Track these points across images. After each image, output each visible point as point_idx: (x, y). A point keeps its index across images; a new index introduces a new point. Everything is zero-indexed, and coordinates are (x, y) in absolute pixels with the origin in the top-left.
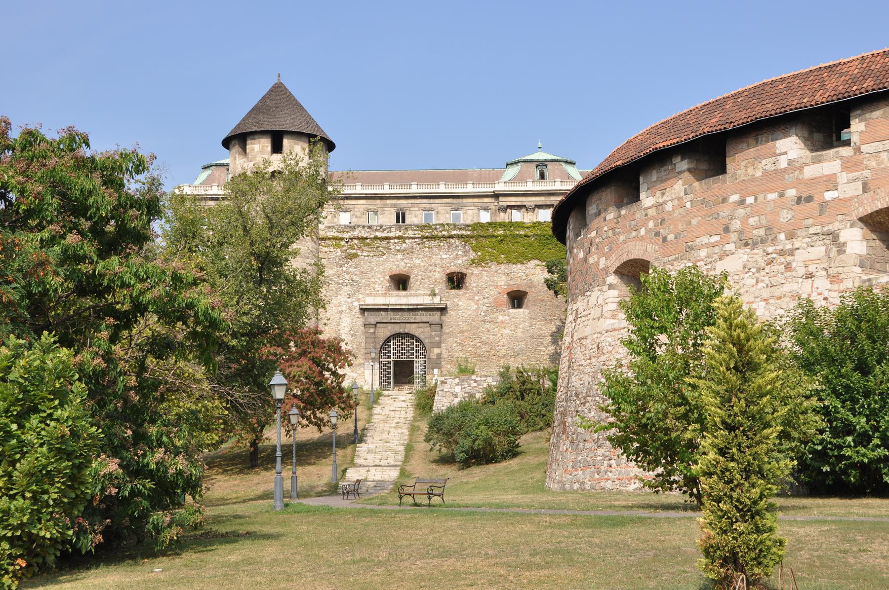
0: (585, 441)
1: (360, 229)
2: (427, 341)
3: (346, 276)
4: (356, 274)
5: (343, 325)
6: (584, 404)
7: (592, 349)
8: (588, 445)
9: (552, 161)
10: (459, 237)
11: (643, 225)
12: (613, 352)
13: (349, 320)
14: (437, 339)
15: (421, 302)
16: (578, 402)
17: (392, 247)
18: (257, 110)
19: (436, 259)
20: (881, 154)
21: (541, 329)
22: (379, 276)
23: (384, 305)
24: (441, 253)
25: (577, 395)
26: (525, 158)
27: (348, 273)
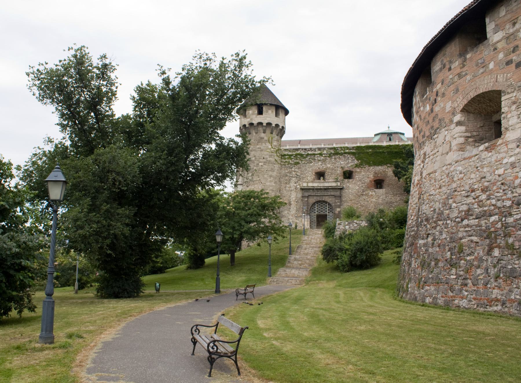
2: (333, 205)
5: (292, 197)
6: (435, 228)
7: (441, 179)
10: (349, 153)
11: (491, 60)
12: (464, 179)
14: (338, 203)
15: (331, 185)
16: (428, 226)
17: (316, 158)
19: (338, 164)
20: (458, 197)
23: (312, 187)
27: (295, 171)
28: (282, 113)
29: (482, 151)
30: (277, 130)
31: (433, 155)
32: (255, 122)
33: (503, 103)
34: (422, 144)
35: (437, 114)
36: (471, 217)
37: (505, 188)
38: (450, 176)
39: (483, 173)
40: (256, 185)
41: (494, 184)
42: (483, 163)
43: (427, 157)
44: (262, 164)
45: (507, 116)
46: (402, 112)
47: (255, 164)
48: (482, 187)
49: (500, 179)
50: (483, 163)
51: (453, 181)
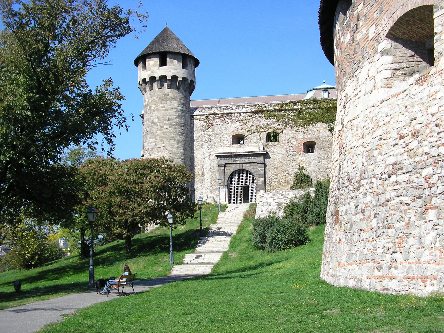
0: (361, 230)
1: (214, 108)
2: (256, 174)
3: (207, 136)
4: (212, 135)
5: (205, 166)
6: (358, 189)
8: (364, 235)
9: (331, 88)
12: (391, 123)
13: (209, 163)
18: (153, 43)
21: (325, 164)
22: (226, 136)
23: (229, 153)
24: (263, 121)
25: (350, 180)
26: (317, 88)
27: (208, 135)
28: (190, 63)
29: (412, 84)
31: (354, 97)
32: (157, 76)
33: (435, 21)
34: (343, 85)
35: (359, 44)
36: (400, 172)
37: (439, 131)
38: (374, 120)
39: (414, 113)
41: (427, 126)
42: (414, 100)
43: (349, 99)
45: (440, 37)
46: (323, 49)
47: (159, 127)
48: (413, 132)
49: (434, 118)
50: (414, 100)
51: (378, 127)
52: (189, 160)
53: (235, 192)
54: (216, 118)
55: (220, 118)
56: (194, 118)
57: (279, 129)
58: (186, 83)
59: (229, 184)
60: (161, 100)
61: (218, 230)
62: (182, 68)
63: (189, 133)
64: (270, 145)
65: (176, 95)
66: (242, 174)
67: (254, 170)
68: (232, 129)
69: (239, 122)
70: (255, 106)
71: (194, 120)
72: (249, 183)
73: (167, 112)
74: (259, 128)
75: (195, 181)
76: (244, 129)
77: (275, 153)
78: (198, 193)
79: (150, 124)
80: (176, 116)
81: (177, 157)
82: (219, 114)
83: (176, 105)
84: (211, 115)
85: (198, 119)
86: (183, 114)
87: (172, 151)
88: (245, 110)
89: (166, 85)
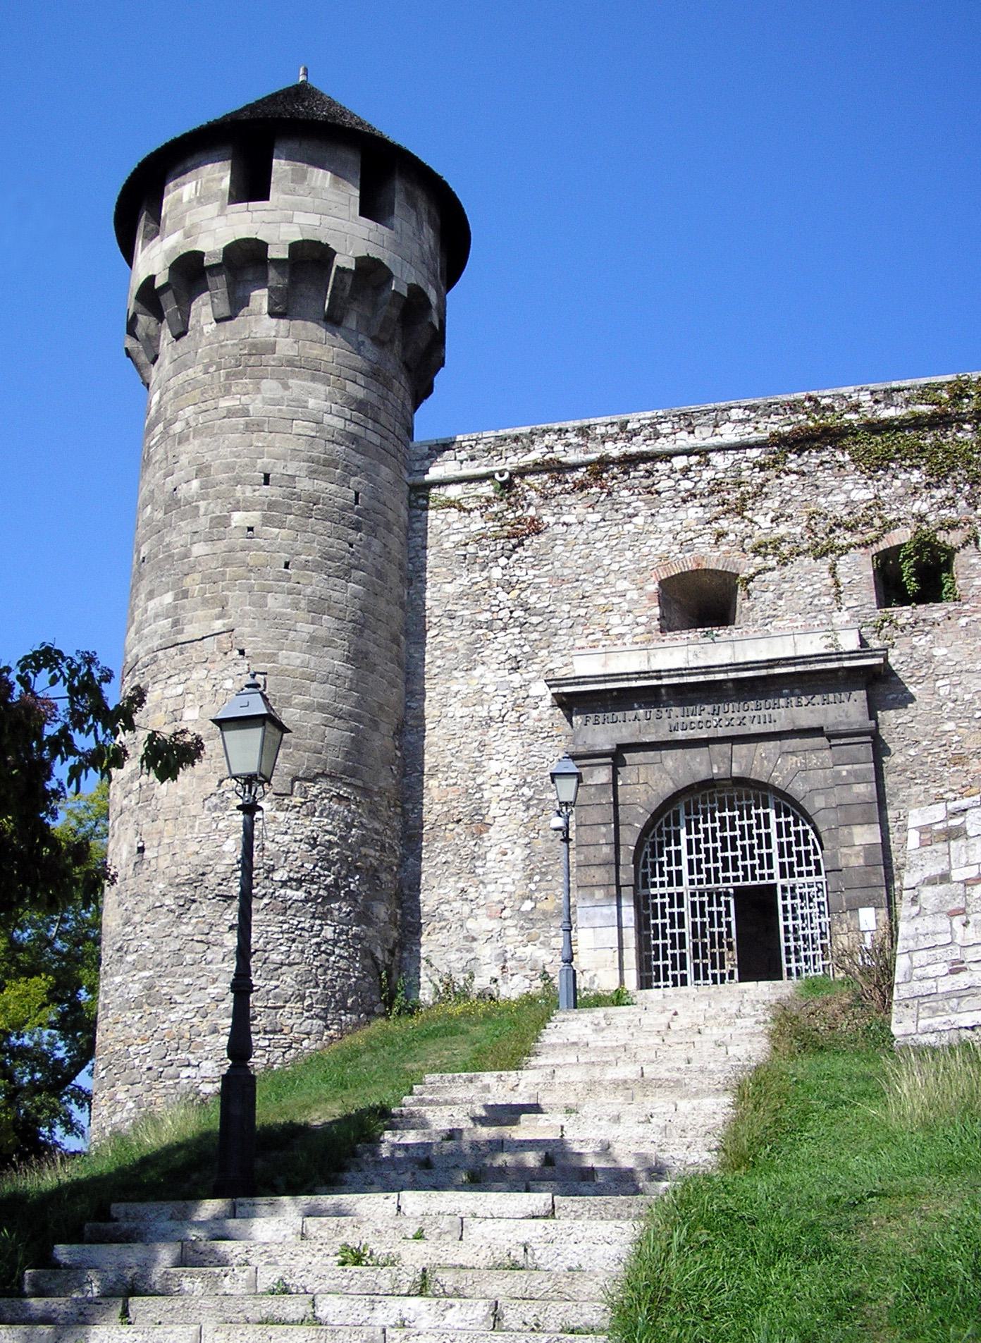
2: (819, 802)
3: (502, 596)
4: (538, 588)
5: (494, 767)
13: (515, 748)
22: (622, 585)
23: (640, 675)
24: (849, 486)
27: (509, 586)
30: (375, 306)
32: (212, 245)
40: (198, 674)
44: (254, 517)
47: (203, 523)
52: (386, 728)
53: (687, 930)
54: (558, 488)
55: (582, 486)
56: (427, 498)
57: (953, 526)
58: (386, 295)
59: (642, 882)
60: (228, 376)
61: (486, 1133)
62: (361, 214)
63: (394, 577)
64: (901, 621)
65: (316, 351)
66: (727, 814)
67: (805, 780)
68: (659, 545)
69: (696, 502)
70: (794, 407)
71: (426, 508)
72: (776, 870)
73: (257, 440)
74: (821, 527)
75: (424, 865)
76: (731, 537)
77: (942, 670)
78: (441, 937)
79: (159, 515)
80: (311, 460)
81: (307, 699)
82: (574, 467)
83: (312, 403)
84: (532, 473)
85: (450, 504)
86: (359, 459)
87: (272, 658)
88: (729, 434)
89: (260, 298)
